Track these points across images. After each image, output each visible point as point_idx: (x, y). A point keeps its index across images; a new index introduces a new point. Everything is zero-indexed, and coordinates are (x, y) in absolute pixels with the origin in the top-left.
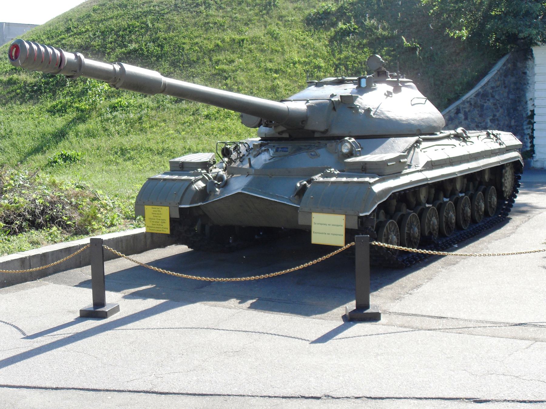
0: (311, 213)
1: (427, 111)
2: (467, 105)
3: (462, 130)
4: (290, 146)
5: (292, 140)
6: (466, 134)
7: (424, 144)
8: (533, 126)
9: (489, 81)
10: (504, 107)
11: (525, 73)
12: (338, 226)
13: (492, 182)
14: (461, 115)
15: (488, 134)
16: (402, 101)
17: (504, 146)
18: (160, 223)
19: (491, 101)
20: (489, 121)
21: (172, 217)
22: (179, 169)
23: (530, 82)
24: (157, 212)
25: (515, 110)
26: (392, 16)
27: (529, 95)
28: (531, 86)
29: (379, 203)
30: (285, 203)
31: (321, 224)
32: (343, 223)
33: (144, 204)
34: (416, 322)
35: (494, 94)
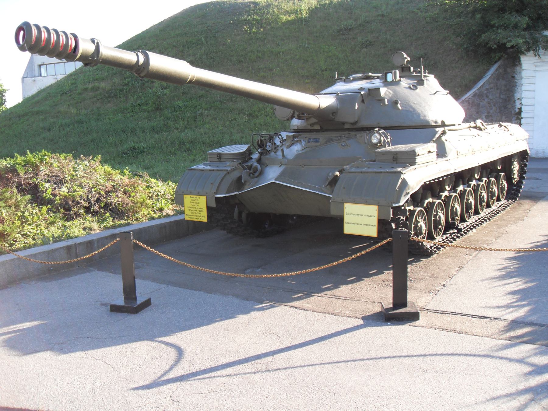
0: (343, 203)
4: (322, 137)
5: (323, 132)
8: (521, 121)
9: (484, 84)
10: (497, 105)
11: (514, 77)
12: (370, 216)
16: (434, 100)
18: (198, 212)
19: (486, 100)
21: (209, 206)
22: (217, 160)
23: (517, 84)
24: (195, 201)
25: (505, 107)
26: (401, 32)
27: (517, 96)
28: (519, 88)
30: (317, 192)
31: (354, 215)
32: (376, 213)
33: (184, 193)
34: (458, 323)
35: (488, 94)
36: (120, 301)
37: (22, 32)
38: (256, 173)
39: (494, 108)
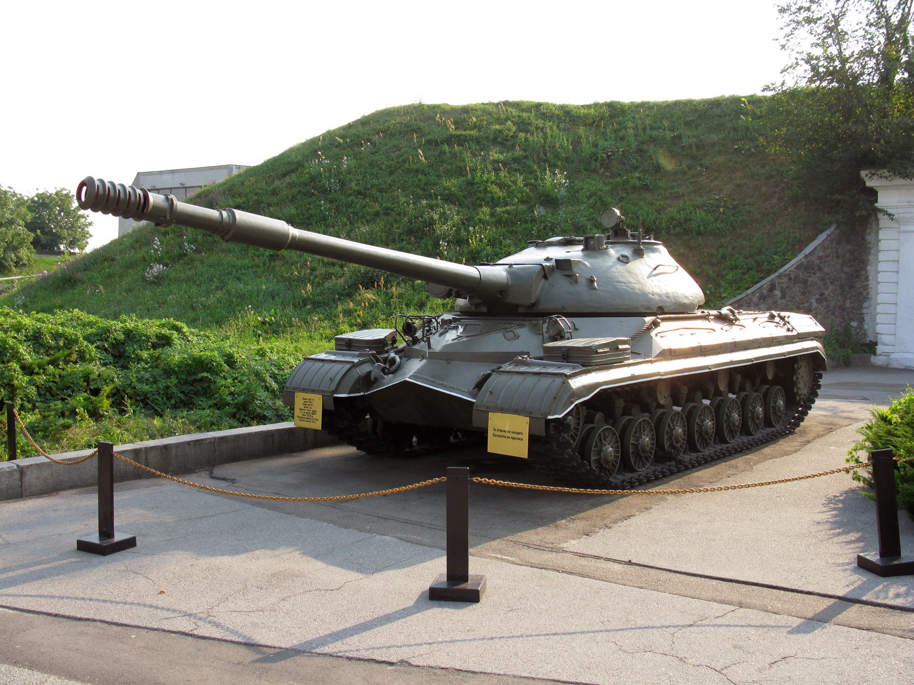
1: (681, 284)
2: (785, 279)
3: (729, 310)
6: (734, 316)
7: (664, 326)
9: (815, 249)
11: (864, 239)
13: (776, 381)
14: (777, 293)
15: (772, 317)
16: (660, 273)
17: (795, 333)
19: (818, 275)
20: (814, 301)
25: (852, 287)
29: (576, 402)
35: (822, 266)
37: (85, 188)
38: (392, 367)
39: (831, 287)
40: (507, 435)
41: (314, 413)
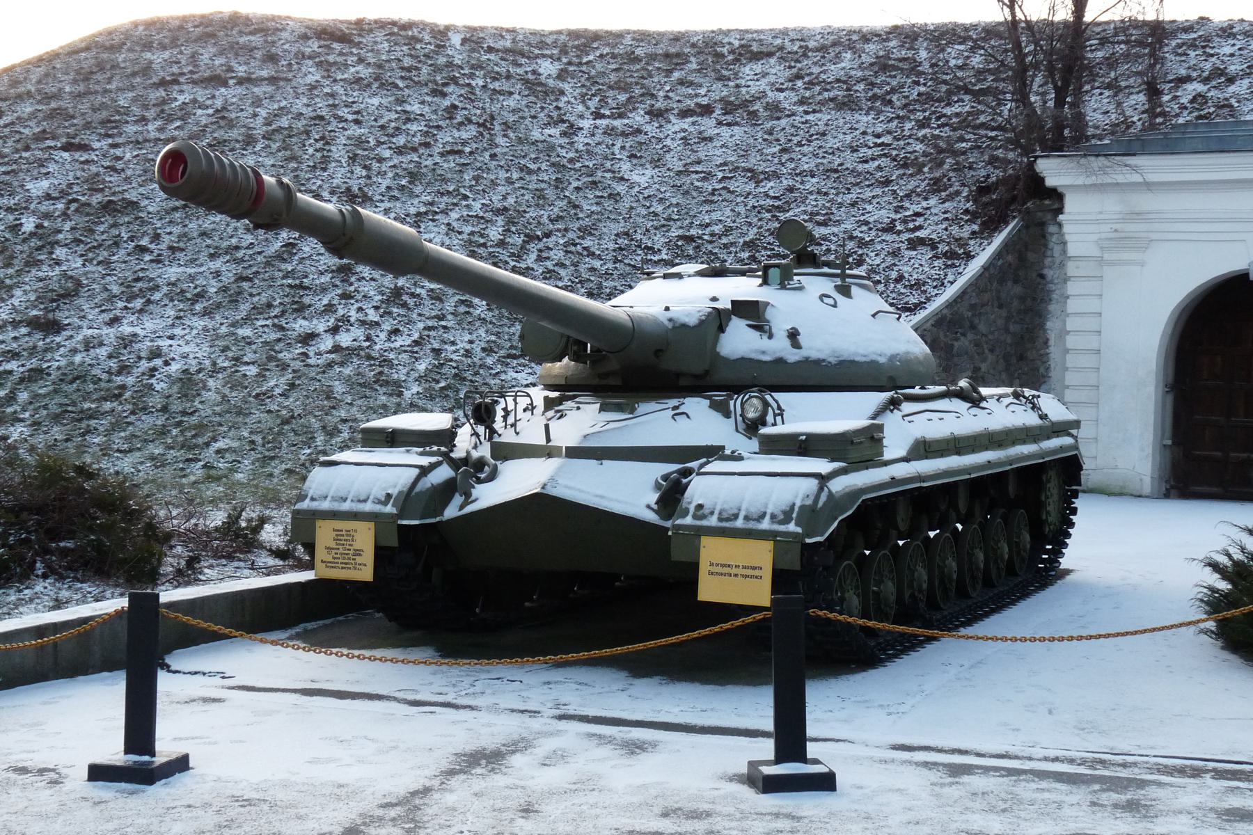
7: (907, 407)
11: (1042, 276)
25: (1021, 358)
27: (1052, 325)
35: (976, 321)
36: (113, 751)
39: (991, 358)
40: (734, 571)
41: (358, 553)
